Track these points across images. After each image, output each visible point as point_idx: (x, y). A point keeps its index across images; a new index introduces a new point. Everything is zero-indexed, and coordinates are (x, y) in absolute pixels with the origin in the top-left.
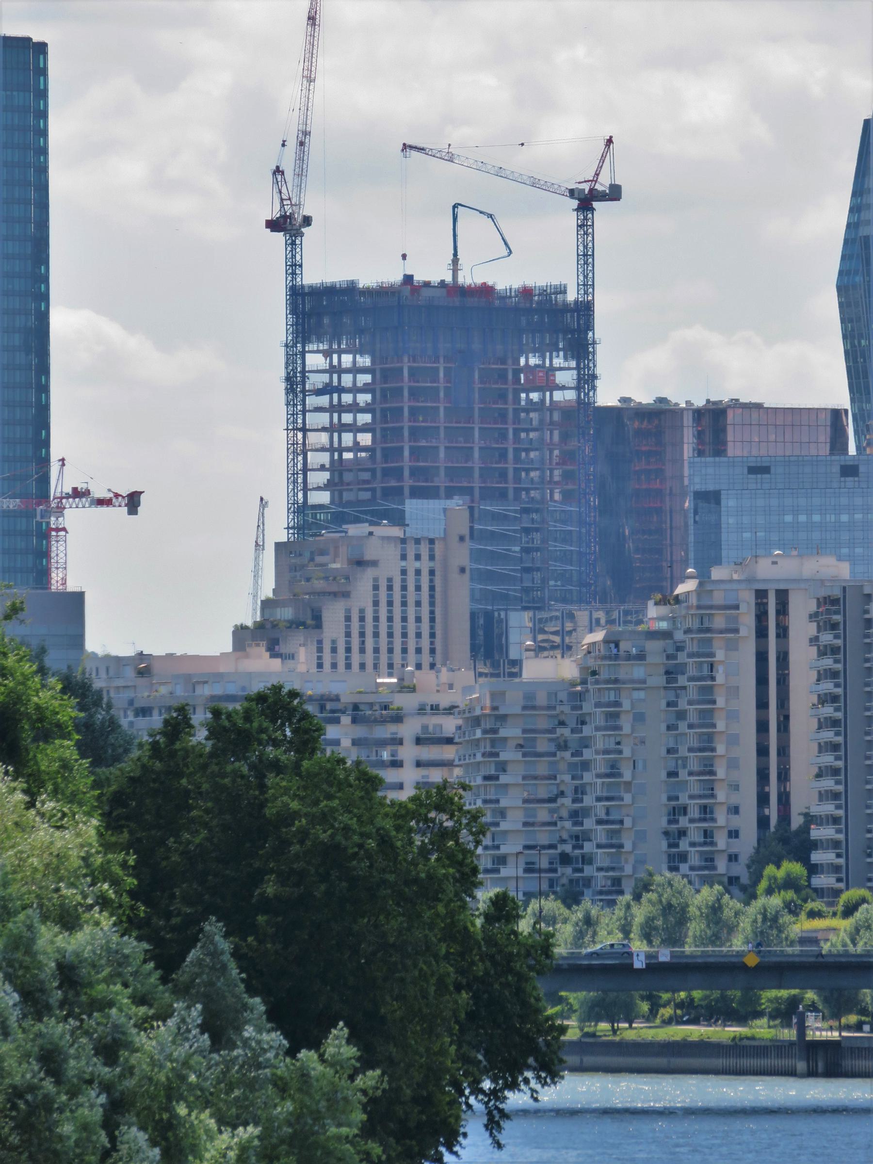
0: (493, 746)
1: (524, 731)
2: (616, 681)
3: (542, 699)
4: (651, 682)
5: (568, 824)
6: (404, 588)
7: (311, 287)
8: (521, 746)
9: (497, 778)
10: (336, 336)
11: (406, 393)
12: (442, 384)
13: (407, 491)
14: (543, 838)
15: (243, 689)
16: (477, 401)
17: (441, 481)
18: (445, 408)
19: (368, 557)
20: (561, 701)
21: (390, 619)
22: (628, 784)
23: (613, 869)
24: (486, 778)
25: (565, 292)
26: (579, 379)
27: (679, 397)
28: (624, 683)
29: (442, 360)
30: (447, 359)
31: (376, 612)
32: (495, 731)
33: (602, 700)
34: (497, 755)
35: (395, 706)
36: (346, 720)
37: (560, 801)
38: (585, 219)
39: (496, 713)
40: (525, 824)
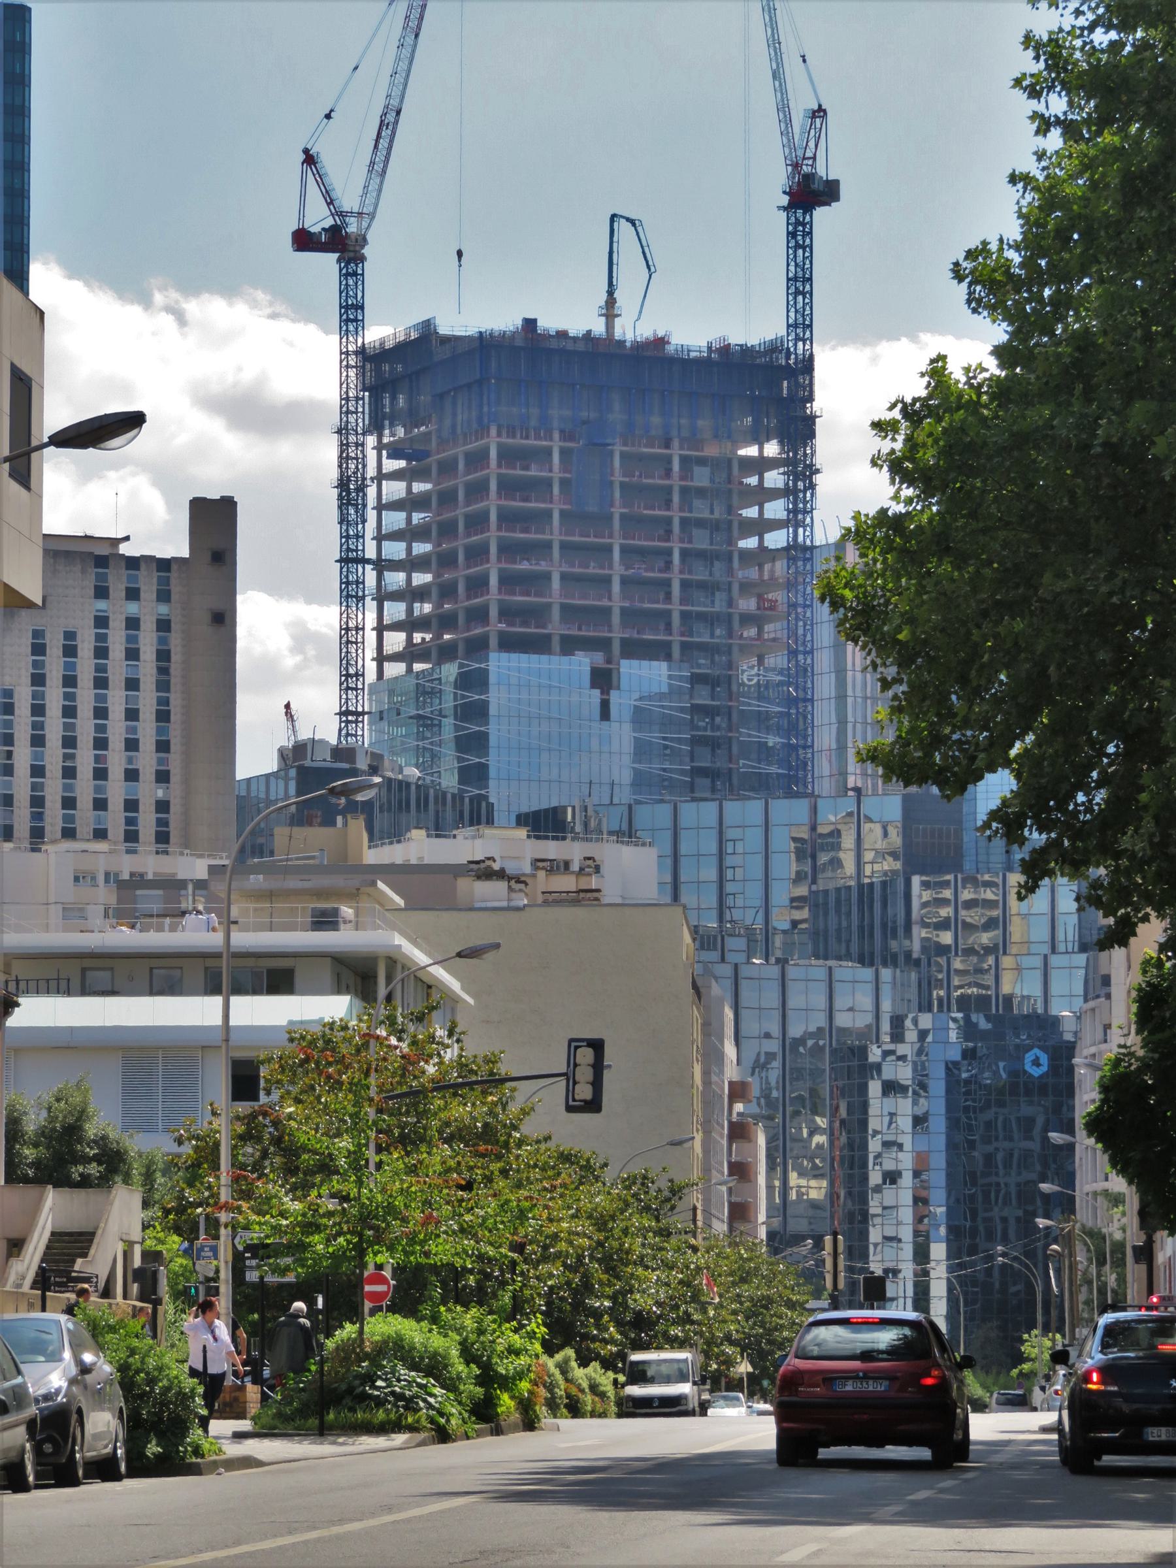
6: (101, 652)
12: (557, 473)
13: (493, 642)
16: (617, 503)
17: (556, 627)
18: (563, 513)
21: (69, 712)
30: (566, 436)
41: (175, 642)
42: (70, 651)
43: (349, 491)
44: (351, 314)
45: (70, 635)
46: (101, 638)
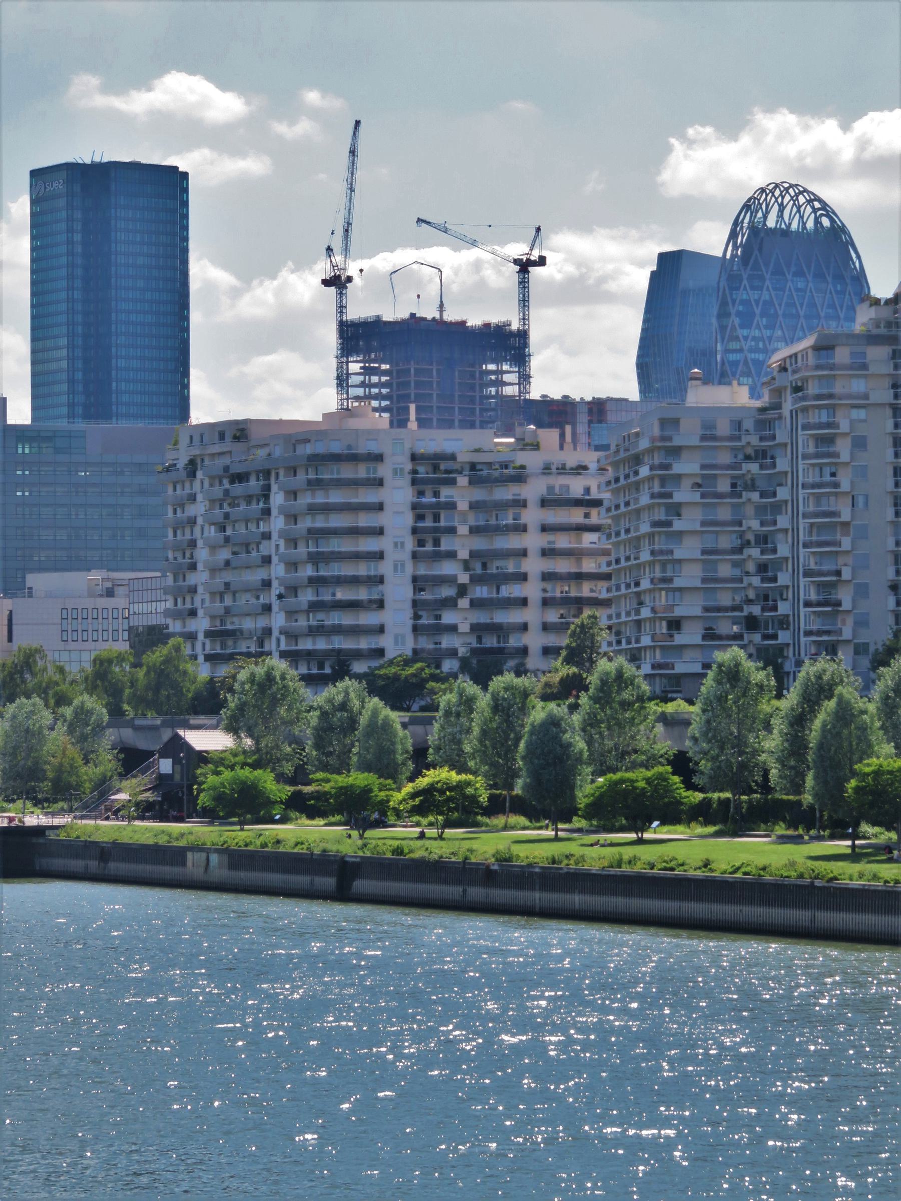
0: (662, 486)
1: (703, 467)
2: (831, 396)
3: (723, 428)
4: (875, 398)
5: (756, 581)
7: (352, 322)
8: (699, 486)
9: (669, 524)
10: (368, 352)
11: (413, 384)
12: (435, 379)
14: (725, 599)
15: (349, 447)
18: (438, 395)
20: (747, 431)
22: (846, 525)
23: (828, 632)
24: (655, 524)
25: (510, 325)
26: (519, 378)
27: (576, 396)
28: (840, 399)
29: (435, 364)
32: (668, 467)
33: (811, 420)
34: (669, 495)
35: (518, 464)
36: (462, 481)
37: (747, 552)
38: (524, 278)
39: (668, 444)
40: (704, 580)
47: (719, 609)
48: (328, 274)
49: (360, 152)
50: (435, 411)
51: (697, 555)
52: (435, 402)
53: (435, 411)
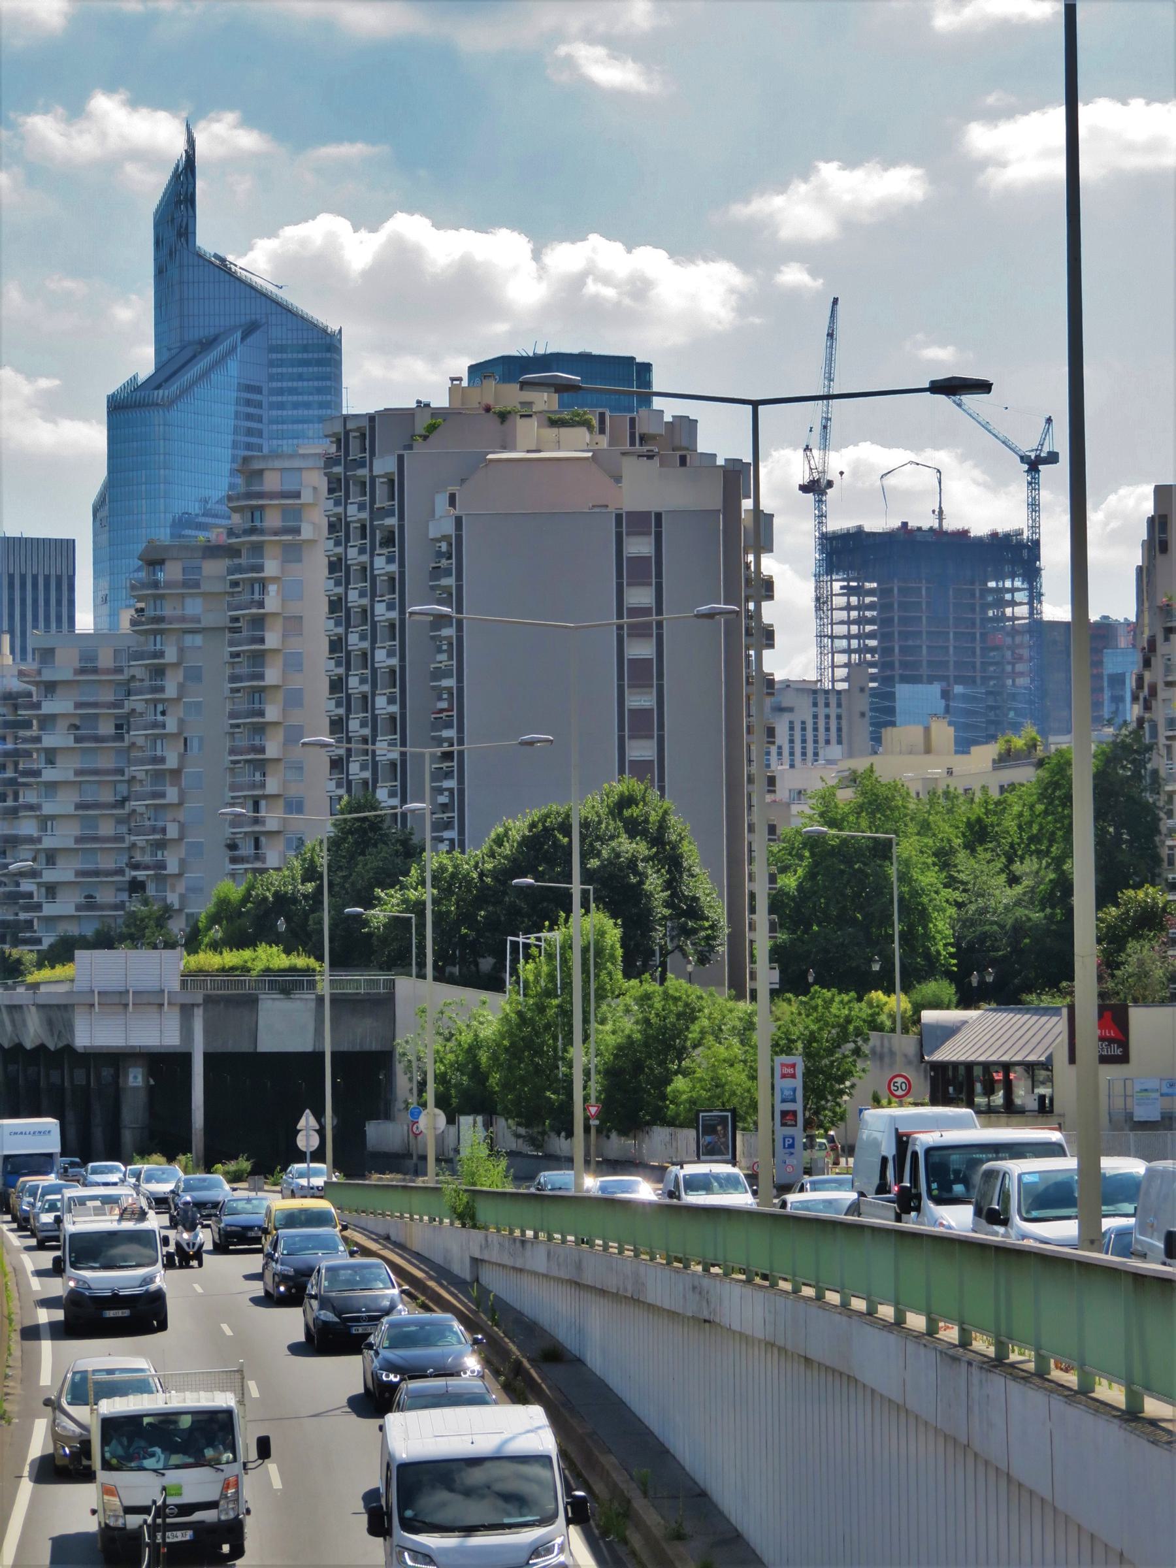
1: (78, 705)
6: (816, 729)
7: (834, 533)
8: (77, 728)
11: (896, 606)
13: (897, 678)
14: (107, 863)
17: (924, 671)
19: (784, 705)
31: (792, 748)
41: (844, 723)
42: (804, 729)
43: (821, 602)
44: (821, 516)
45: (803, 723)
46: (815, 723)
47: (96, 873)
48: (805, 478)
49: (839, 334)
50: (924, 636)
51: (71, 810)
52: (924, 626)
53: (924, 636)
